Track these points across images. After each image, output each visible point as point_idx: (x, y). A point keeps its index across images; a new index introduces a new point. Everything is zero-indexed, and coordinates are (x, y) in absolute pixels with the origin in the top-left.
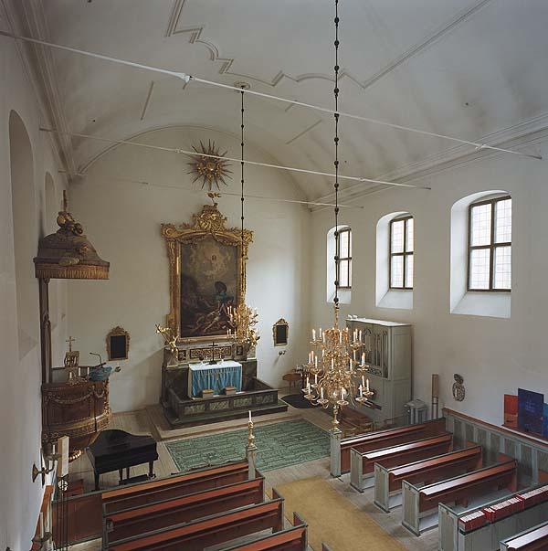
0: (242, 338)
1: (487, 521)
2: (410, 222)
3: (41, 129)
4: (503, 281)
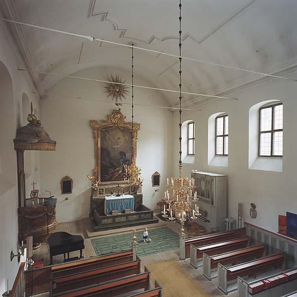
0: (132, 183)
2: (227, 118)
4: (278, 151)
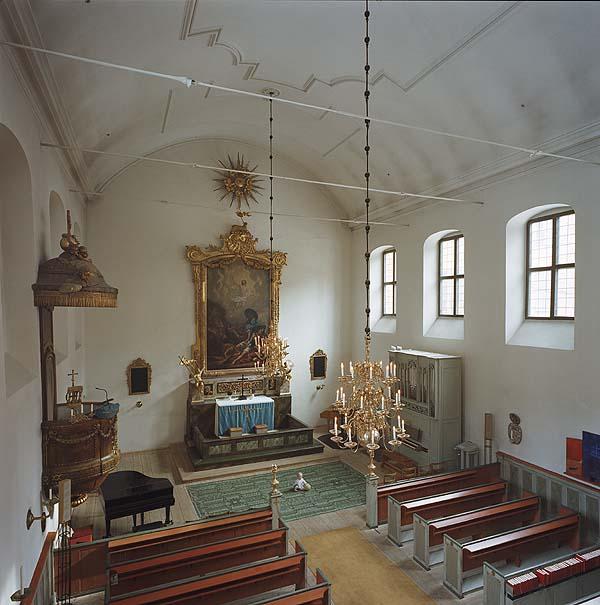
1: (540, 585)
2: (461, 241)
3: (42, 144)
4: (566, 307)
